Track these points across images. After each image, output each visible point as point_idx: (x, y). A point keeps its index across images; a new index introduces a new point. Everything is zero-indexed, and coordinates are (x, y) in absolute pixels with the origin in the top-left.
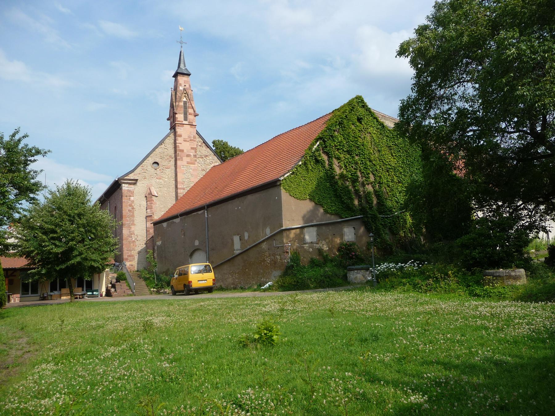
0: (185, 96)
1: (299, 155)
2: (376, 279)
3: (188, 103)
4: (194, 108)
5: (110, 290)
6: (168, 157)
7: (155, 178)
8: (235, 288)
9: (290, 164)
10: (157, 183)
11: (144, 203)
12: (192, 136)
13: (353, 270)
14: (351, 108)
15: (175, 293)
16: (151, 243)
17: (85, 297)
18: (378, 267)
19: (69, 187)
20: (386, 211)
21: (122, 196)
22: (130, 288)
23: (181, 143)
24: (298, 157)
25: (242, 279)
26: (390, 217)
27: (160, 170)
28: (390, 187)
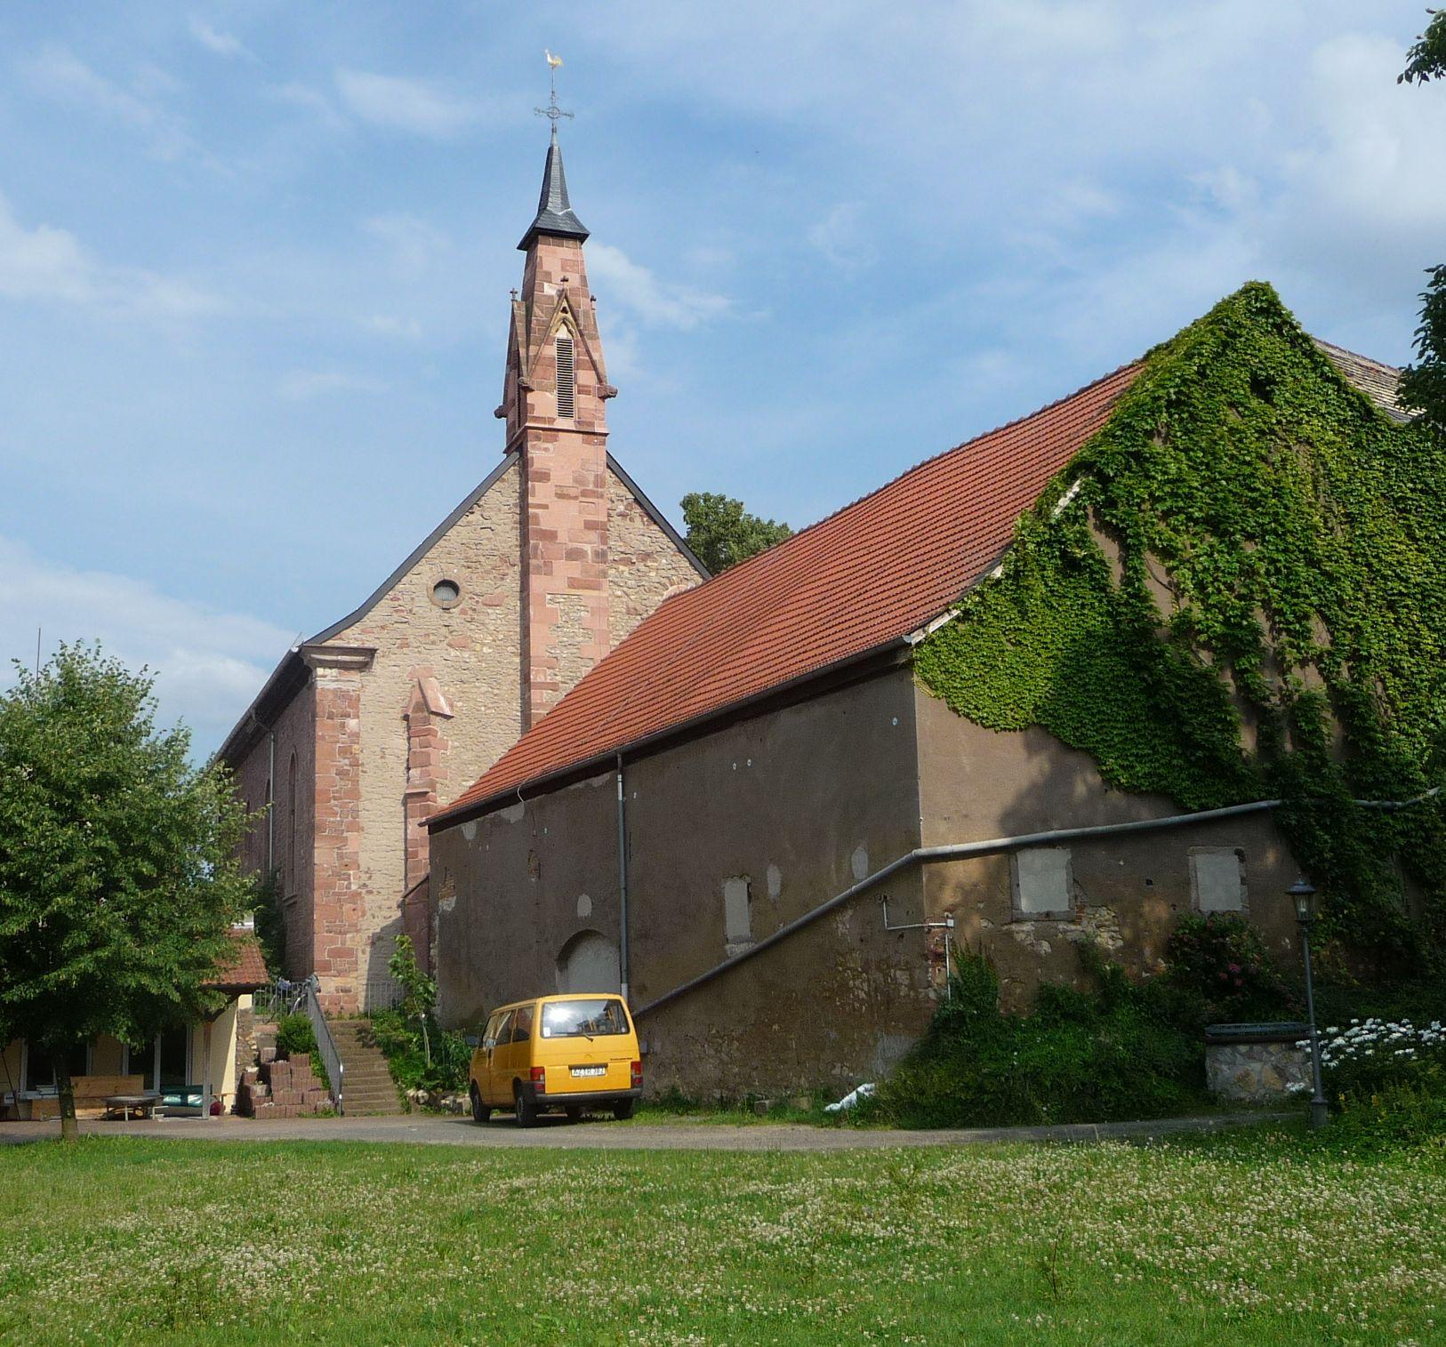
0: (564, 322)
1: (997, 539)
2: (1324, 1095)
3: (576, 346)
5: (248, 1089)
6: (495, 561)
7: (444, 645)
8: (725, 1105)
9: (956, 580)
11: (399, 743)
12: (592, 479)
13: (1233, 1041)
14: (1224, 337)
15: (482, 1116)
16: (419, 900)
17: (153, 1116)
18: (1336, 1035)
19: (68, 676)
20: (1385, 783)
21: (314, 716)
22: (327, 1085)
23: (545, 507)
24: (990, 549)
25: (754, 1064)
26: (1401, 809)
27: (463, 612)
28: (1401, 676)
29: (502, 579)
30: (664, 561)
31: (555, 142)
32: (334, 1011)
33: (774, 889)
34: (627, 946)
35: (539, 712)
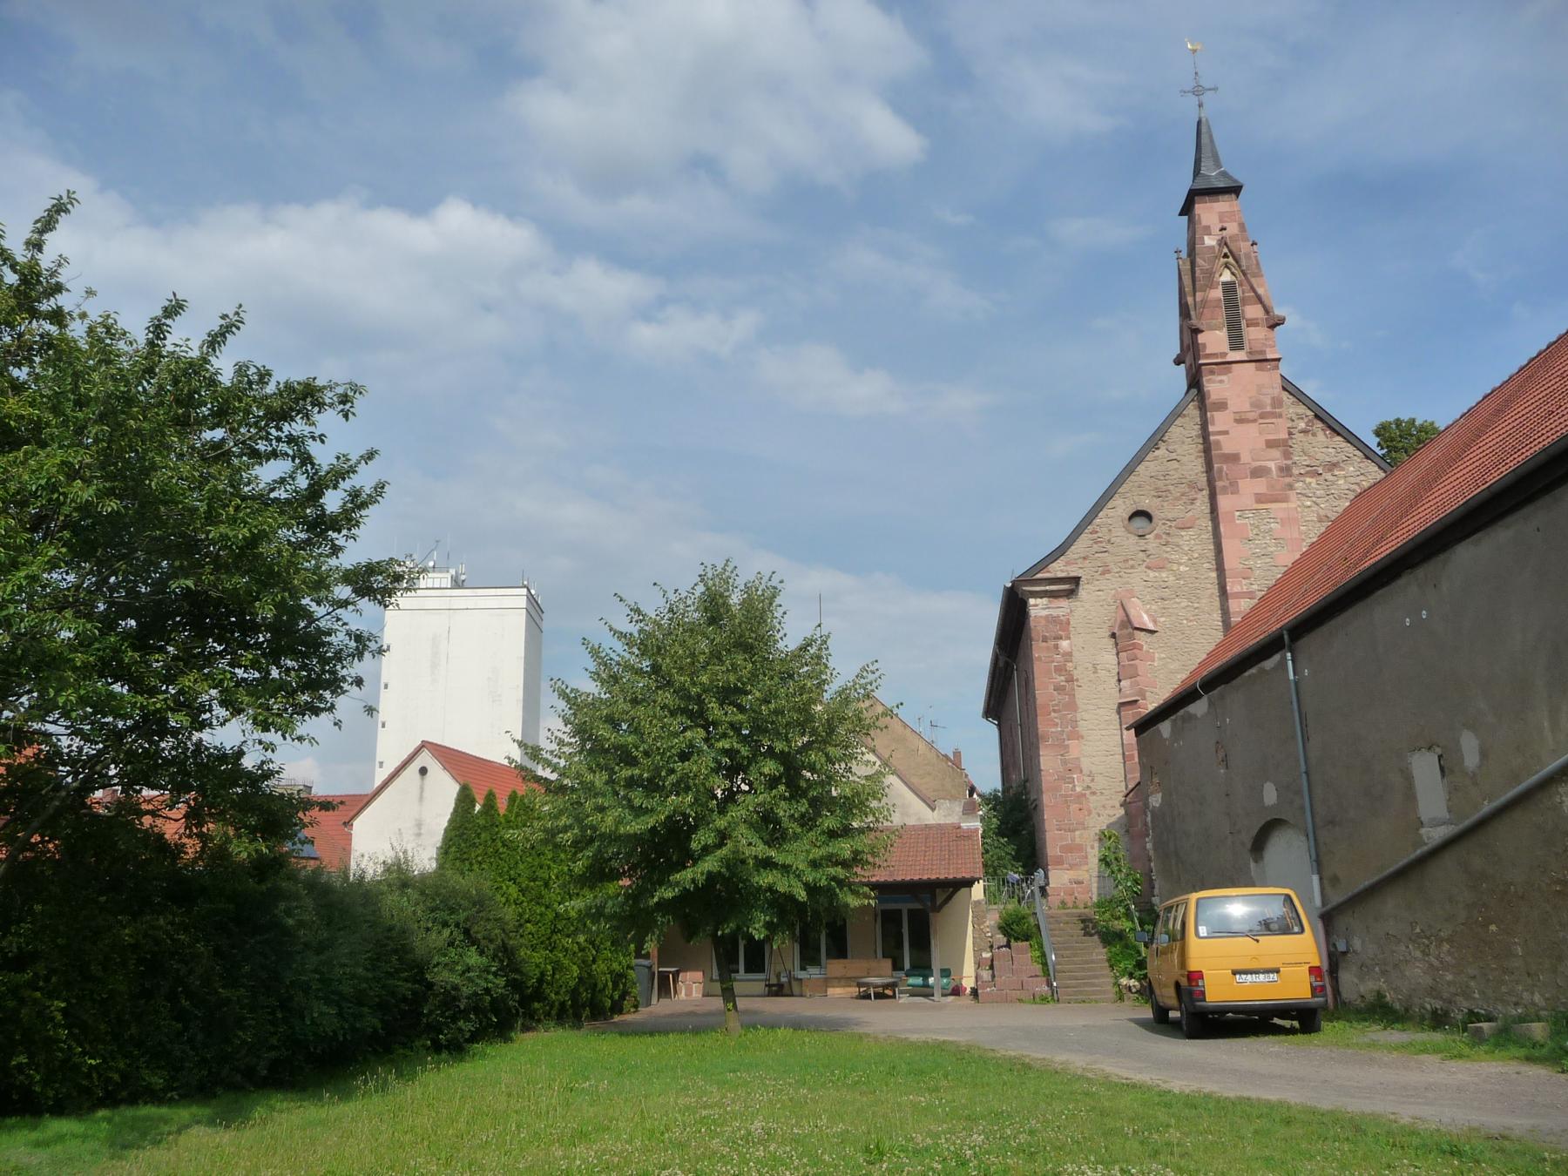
0: (1227, 266)
4: (1264, 299)
6: (1185, 489)
7: (1143, 568)
8: (1438, 1020)
10: (1150, 584)
11: (1109, 658)
12: (1269, 401)
16: (1135, 797)
23: (1226, 433)
25: (1471, 971)
29: (1192, 503)
30: (1352, 469)
31: (1202, 115)
32: (1069, 901)
33: (1471, 760)
34: (1314, 833)
35: (1235, 619)
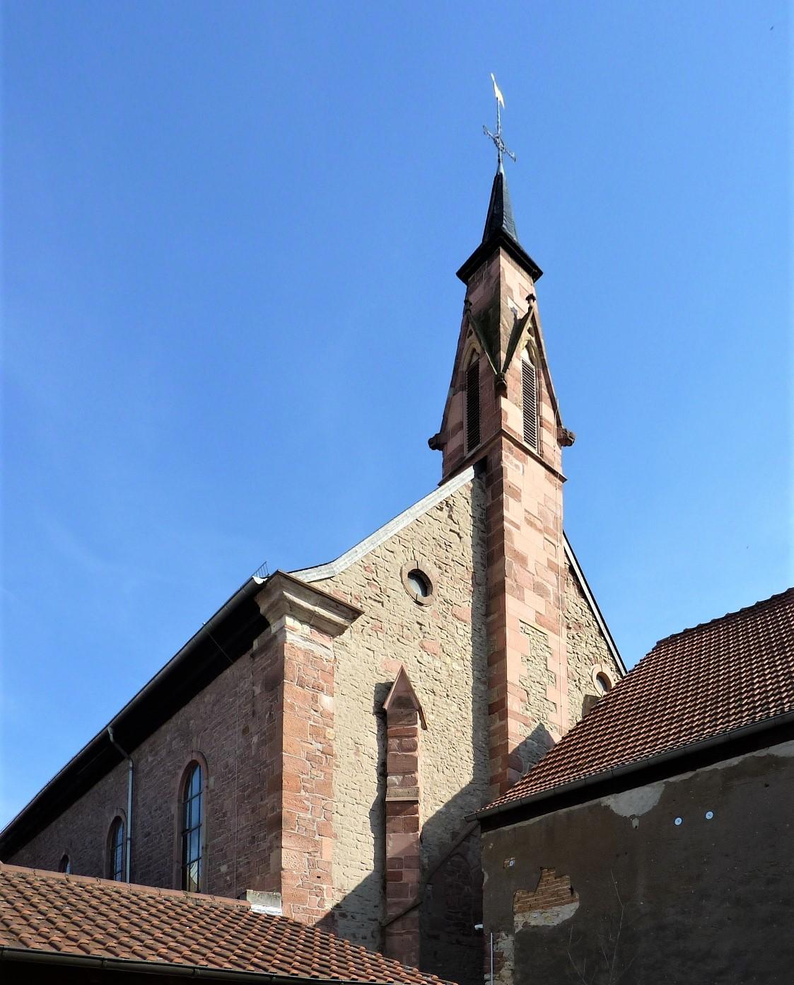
23: (518, 527)
